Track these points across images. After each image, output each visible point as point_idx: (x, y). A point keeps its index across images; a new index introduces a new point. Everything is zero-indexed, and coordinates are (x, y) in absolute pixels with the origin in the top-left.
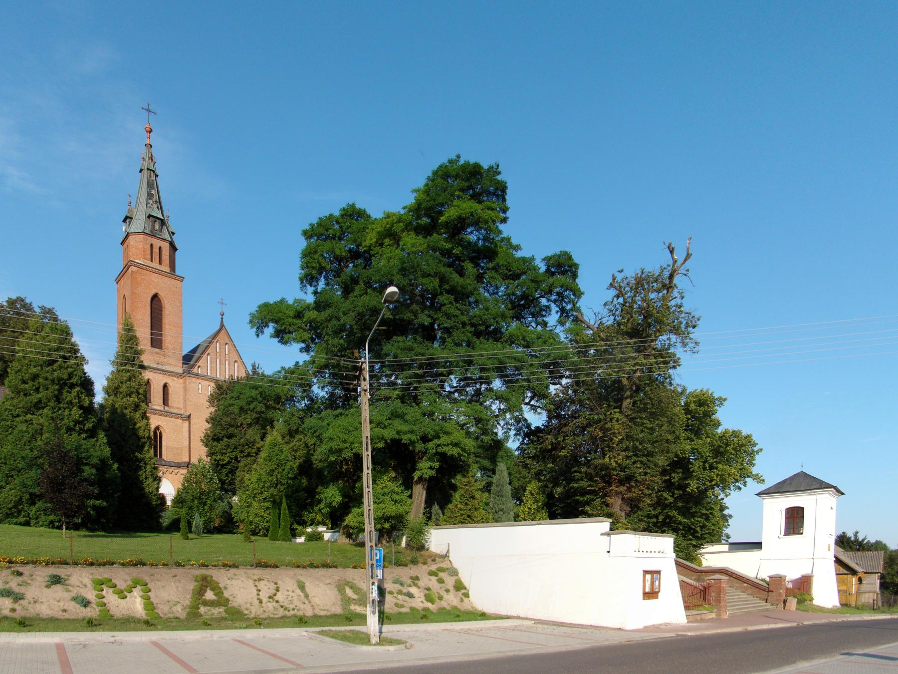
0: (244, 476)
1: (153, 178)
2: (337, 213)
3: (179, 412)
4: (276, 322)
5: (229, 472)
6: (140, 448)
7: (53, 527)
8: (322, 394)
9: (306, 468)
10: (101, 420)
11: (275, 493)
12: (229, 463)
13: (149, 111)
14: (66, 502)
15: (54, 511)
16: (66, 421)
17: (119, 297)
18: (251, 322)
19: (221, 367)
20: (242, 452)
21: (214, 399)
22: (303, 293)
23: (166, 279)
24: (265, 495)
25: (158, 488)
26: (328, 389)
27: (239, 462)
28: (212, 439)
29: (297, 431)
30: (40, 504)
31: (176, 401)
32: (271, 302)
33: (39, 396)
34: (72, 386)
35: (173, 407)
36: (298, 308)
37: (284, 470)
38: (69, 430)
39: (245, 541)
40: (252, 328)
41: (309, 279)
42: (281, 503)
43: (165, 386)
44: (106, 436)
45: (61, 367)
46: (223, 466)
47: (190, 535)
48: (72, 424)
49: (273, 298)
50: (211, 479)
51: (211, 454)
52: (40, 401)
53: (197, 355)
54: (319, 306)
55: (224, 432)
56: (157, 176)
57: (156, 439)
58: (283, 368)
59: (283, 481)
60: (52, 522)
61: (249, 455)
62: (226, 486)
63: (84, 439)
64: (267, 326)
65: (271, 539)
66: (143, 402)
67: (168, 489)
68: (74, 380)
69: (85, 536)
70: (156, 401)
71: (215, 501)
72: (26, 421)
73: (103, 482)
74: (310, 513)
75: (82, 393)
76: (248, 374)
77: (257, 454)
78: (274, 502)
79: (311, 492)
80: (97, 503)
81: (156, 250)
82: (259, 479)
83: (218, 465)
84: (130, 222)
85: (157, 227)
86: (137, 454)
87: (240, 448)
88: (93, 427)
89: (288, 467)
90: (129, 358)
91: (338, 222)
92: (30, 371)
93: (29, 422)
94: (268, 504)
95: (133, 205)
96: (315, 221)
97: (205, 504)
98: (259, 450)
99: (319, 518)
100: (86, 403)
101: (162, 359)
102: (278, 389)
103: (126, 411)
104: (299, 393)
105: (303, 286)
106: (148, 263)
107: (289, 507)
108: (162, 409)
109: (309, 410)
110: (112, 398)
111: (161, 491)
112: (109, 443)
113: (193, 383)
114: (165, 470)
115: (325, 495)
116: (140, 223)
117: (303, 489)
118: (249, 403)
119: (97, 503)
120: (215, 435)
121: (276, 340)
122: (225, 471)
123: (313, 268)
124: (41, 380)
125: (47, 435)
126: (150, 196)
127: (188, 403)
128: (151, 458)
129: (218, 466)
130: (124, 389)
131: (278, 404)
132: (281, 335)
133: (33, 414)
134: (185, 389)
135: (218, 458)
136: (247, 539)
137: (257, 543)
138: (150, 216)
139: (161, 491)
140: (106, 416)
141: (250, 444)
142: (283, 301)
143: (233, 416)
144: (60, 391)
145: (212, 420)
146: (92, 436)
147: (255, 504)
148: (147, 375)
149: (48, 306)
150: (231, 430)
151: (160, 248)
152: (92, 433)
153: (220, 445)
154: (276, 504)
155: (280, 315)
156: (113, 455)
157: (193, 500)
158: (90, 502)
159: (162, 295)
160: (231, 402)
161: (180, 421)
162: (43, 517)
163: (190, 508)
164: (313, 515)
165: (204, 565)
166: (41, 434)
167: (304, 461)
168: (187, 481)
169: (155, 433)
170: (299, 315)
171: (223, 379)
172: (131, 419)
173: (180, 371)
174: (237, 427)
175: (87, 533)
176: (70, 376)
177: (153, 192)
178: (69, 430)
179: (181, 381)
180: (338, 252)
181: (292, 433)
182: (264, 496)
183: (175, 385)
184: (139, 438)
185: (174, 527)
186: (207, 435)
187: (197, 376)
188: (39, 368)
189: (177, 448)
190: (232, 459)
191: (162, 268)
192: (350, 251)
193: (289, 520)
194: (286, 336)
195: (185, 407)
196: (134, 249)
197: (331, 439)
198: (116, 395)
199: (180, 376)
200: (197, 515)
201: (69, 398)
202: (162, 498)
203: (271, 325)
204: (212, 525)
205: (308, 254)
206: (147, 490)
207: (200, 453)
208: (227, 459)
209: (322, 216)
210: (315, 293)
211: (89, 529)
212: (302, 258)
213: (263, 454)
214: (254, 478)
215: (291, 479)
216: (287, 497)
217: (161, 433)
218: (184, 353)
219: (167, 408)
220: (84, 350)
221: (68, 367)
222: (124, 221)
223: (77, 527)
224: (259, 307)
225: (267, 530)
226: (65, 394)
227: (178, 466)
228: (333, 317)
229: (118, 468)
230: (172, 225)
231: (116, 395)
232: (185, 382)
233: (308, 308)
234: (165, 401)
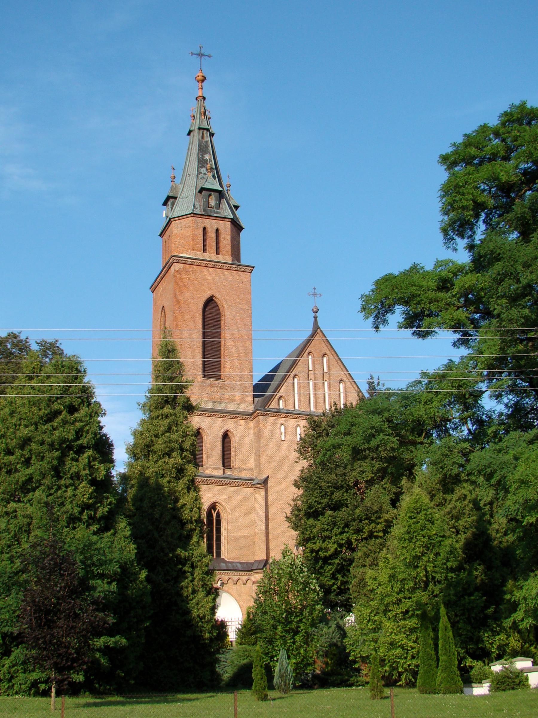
0: (365, 573)
1: (207, 138)
2: (494, 121)
3: (249, 475)
4: (406, 303)
5: (338, 571)
6: (184, 540)
7: (38, 694)
8: (500, 408)
9: (479, 547)
10: (122, 500)
11: (425, 600)
12: (336, 554)
13: (201, 55)
14: (60, 644)
15: (39, 662)
16: (68, 506)
17: (155, 311)
18: (364, 308)
19: (317, 393)
20: (358, 531)
21: (305, 447)
22: (450, 251)
23: (226, 272)
24: (407, 604)
25: (213, 609)
26: (509, 399)
27: (353, 550)
28: (305, 515)
29: (457, 480)
30: (18, 653)
31: (243, 459)
32: (396, 273)
33: (30, 471)
34: (81, 450)
35: (239, 469)
36: (443, 274)
37: (437, 554)
38: (73, 520)
39: (374, 697)
40: (367, 317)
41: (458, 226)
42: (437, 618)
43: (226, 436)
44: (129, 524)
45: (65, 422)
46: (326, 560)
47: (271, 694)
48: (77, 510)
49: (397, 267)
50: (306, 584)
51: (304, 541)
52: (30, 479)
53: (274, 383)
54: (481, 262)
55: (325, 501)
56: (212, 135)
57: (211, 525)
58: (424, 374)
59: (438, 577)
60: (35, 684)
61: (371, 535)
62: (332, 597)
63: (95, 533)
64: (390, 309)
65: (422, 692)
66: (189, 462)
67: (231, 611)
68: (83, 441)
69: (88, 705)
70: (212, 462)
71: (313, 625)
72: (7, 513)
73: (122, 606)
74: (495, 633)
75: (95, 459)
76: (362, 399)
77: (385, 532)
78: (423, 617)
79: (494, 593)
80: (111, 641)
81: (211, 235)
82: (392, 577)
83: (317, 559)
84: (173, 204)
85: (212, 202)
86: (179, 551)
87: (354, 525)
88: (110, 512)
89: (444, 551)
90: (169, 400)
91: (497, 134)
92: (19, 434)
93: (12, 515)
94: (412, 623)
95: (177, 181)
96: (460, 140)
97: (296, 632)
98: (389, 524)
99: (514, 642)
100: (101, 475)
101: (221, 394)
102: (419, 411)
103: (164, 481)
104: (455, 413)
105: (448, 240)
106: (200, 255)
107: (454, 625)
108: (221, 474)
109: (478, 438)
110: (140, 462)
111: (220, 615)
112: (135, 537)
113: (271, 425)
114: (226, 578)
115: (524, 593)
116: (187, 202)
117: (477, 589)
118: (368, 438)
119: (111, 641)
120: (310, 507)
121: (409, 331)
122: (329, 569)
123: (464, 208)
124: (34, 446)
125: (38, 533)
126: (202, 163)
127: (263, 459)
128: (202, 556)
129: (317, 561)
130: (159, 445)
131: (420, 435)
132: (418, 322)
133: (19, 501)
134: (258, 437)
135: (316, 547)
136: (377, 694)
137: (395, 700)
138: (202, 190)
139: (220, 615)
140: (131, 494)
141: (372, 516)
142: (414, 268)
143: (340, 470)
144: (61, 460)
145: (306, 482)
146: (106, 529)
147: (388, 624)
148: (196, 421)
149: (50, 339)
150: (337, 495)
151: (217, 230)
152: (107, 524)
153: (319, 524)
154: (429, 620)
155: (412, 289)
156: (140, 555)
157: (275, 627)
158: (101, 642)
159: (220, 298)
160: (338, 440)
161: (250, 490)
162: (21, 676)
163: (270, 641)
164: (502, 636)
165: (285, 433)
166: (28, 532)
167: (474, 534)
168: (265, 591)
169: (209, 514)
170: (445, 284)
171: (320, 411)
172: (172, 492)
173: (250, 408)
174: (348, 488)
175: (91, 700)
176: (79, 434)
177: (207, 157)
178: (73, 520)
179: (251, 424)
180: (504, 178)
181: (449, 483)
182: (403, 607)
183: (242, 432)
184: (183, 524)
185: (242, 680)
186: (296, 509)
187: (278, 413)
188: (33, 428)
189: (246, 538)
190: (341, 546)
191: (219, 258)
192: (525, 173)
193: (456, 650)
194: (426, 321)
195: (258, 466)
196: (178, 240)
197: (524, 483)
198: (147, 456)
199: (250, 415)
200: (282, 655)
201: (74, 470)
202: (222, 626)
203: (399, 309)
204: (309, 669)
205: (452, 191)
206: (195, 613)
207: (285, 540)
208: (332, 548)
209: (468, 132)
210: (471, 247)
211: (95, 692)
212: (442, 197)
213: (397, 531)
214: (384, 577)
215: (452, 570)
216: (447, 605)
217: (218, 515)
218: (255, 381)
219: (228, 472)
220: (101, 395)
221: (75, 421)
222: (165, 203)
223: (74, 690)
224: (377, 283)
225: (415, 674)
226: (68, 462)
227: (248, 568)
228: (505, 275)
229: (148, 578)
230: (235, 197)
231: (147, 456)
232: (257, 425)
233: (459, 270)
234: (226, 461)
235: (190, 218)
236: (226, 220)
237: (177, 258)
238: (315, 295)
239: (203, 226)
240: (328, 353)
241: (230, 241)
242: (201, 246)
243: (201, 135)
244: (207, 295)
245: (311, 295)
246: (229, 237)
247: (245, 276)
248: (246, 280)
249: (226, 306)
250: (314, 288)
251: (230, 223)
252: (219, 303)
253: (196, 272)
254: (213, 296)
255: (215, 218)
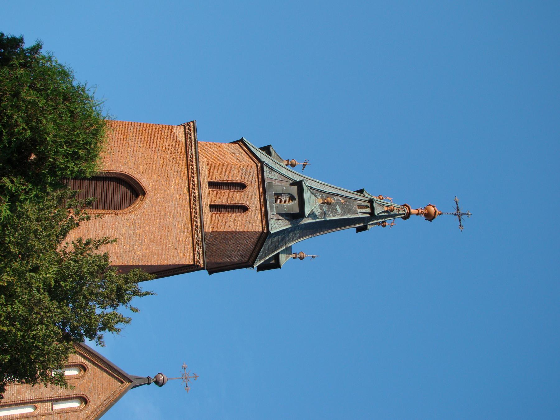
81: (236, 197)
159: (144, 206)
235: (253, 163)
236: (264, 222)
237: (192, 129)
238: (186, 379)
239: (247, 183)
240: (91, 406)
241: (234, 230)
242: (217, 178)
243: (363, 204)
244: (145, 182)
245: (183, 371)
246: (240, 230)
247: (187, 254)
248: (181, 255)
249: (132, 216)
250: (195, 377)
251: (260, 230)
252: (135, 205)
253: (177, 164)
254: (144, 193)
255: (262, 203)
